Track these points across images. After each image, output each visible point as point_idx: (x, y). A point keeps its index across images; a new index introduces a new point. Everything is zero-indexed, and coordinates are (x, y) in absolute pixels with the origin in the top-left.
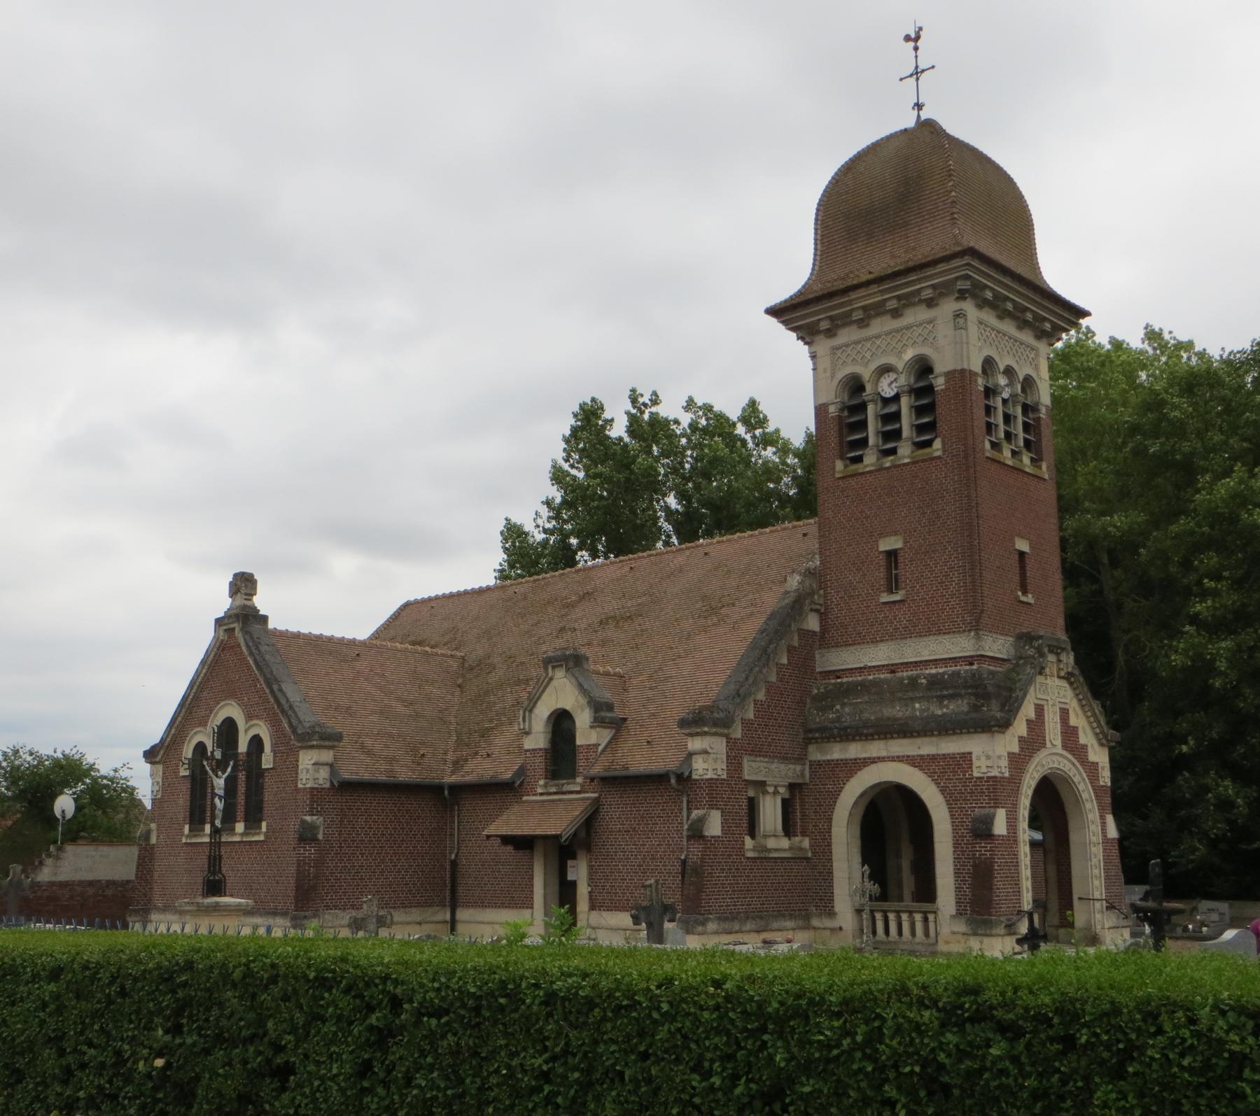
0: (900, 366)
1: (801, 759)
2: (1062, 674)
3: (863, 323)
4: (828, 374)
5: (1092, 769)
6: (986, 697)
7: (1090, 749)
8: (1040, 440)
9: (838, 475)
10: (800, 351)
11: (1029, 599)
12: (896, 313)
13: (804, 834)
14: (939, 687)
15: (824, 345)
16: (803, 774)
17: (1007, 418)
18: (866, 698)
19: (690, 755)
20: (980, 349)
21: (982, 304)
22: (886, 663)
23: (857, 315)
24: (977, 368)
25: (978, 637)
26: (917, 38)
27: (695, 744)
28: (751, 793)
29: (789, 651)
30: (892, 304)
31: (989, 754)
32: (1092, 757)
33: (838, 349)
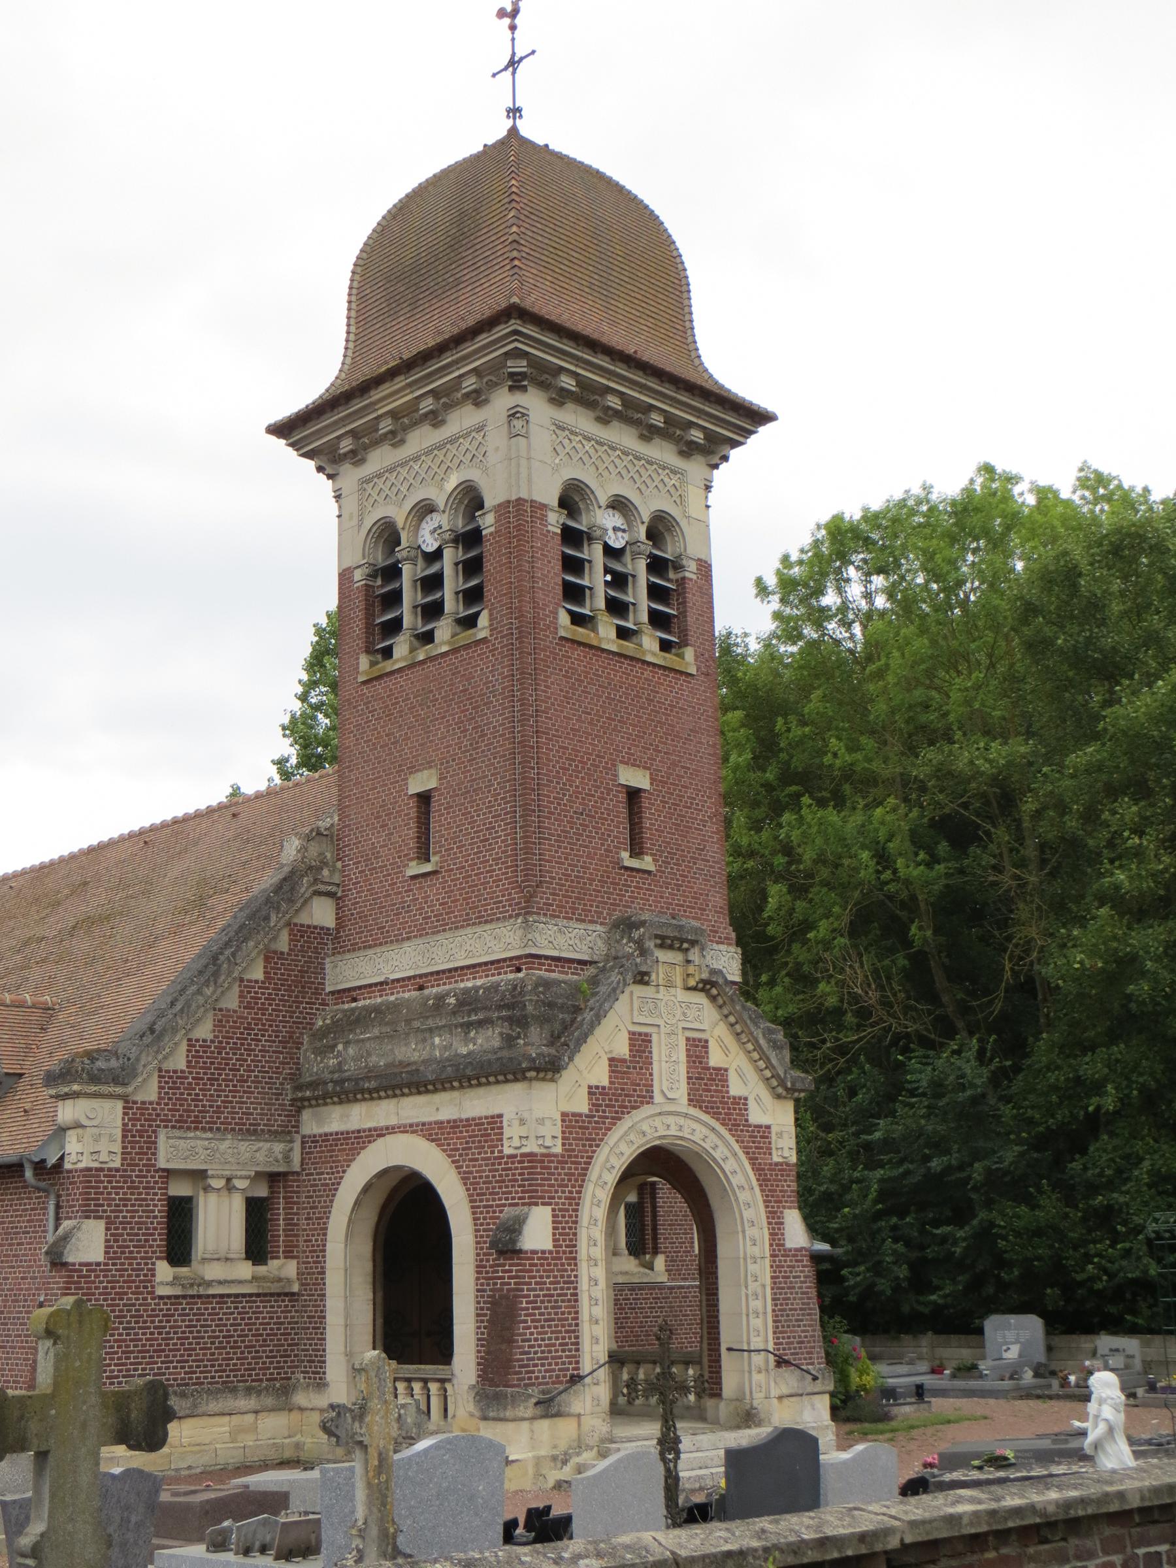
0: (441, 502)
1: (286, 1132)
2: (692, 983)
3: (395, 438)
4: (355, 522)
5: (756, 1140)
6: (520, 1022)
7: (752, 1104)
8: (683, 614)
9: (361, 679)
10: (325, 485)
11: (647, 863)
12: (435, 419)
13: (289, 1255)
14: (470, 1010)
15: (351, 475)
16: (287, 1158)
17: (619, 581)
18: (376, 1032)
19: (63, 1130)
20: (556, 469)
21: (560, 398)
22: (411, 973)
23: (386, 426)
24: (551, 497)
25: (526, 925)
26: (515, 13)
27: (67, 1112)
28: (179, 1189)
29: (267, 959)
30: (427, 405)
31: (531, 1115)
32: (756, 1116)
33: (368, 481)
